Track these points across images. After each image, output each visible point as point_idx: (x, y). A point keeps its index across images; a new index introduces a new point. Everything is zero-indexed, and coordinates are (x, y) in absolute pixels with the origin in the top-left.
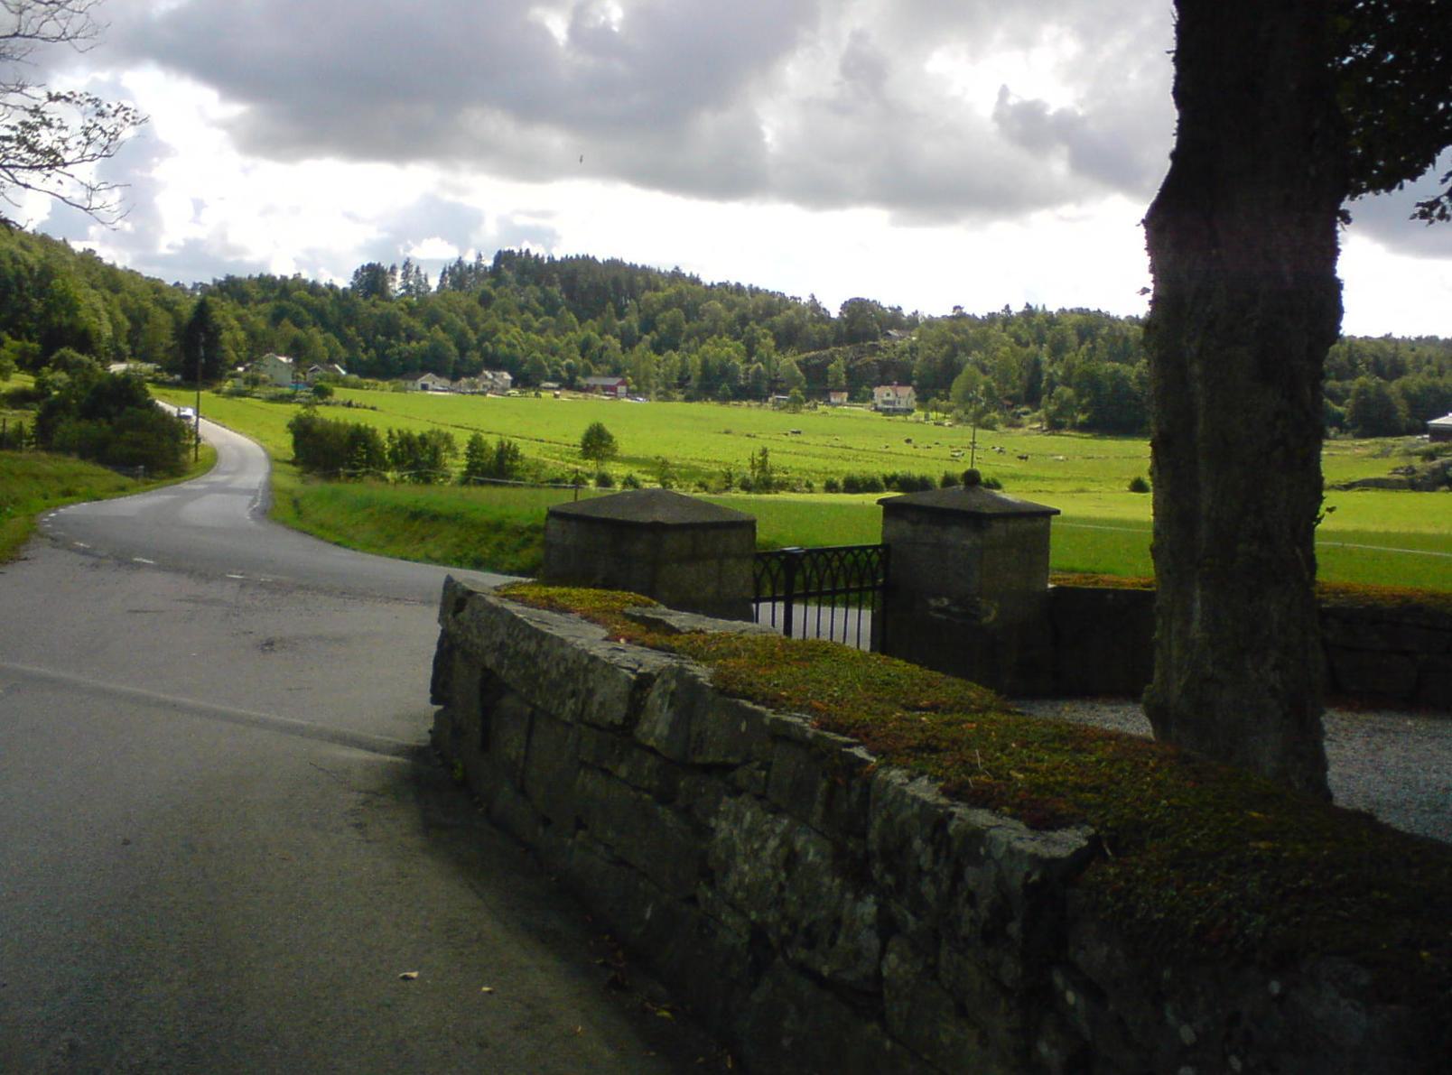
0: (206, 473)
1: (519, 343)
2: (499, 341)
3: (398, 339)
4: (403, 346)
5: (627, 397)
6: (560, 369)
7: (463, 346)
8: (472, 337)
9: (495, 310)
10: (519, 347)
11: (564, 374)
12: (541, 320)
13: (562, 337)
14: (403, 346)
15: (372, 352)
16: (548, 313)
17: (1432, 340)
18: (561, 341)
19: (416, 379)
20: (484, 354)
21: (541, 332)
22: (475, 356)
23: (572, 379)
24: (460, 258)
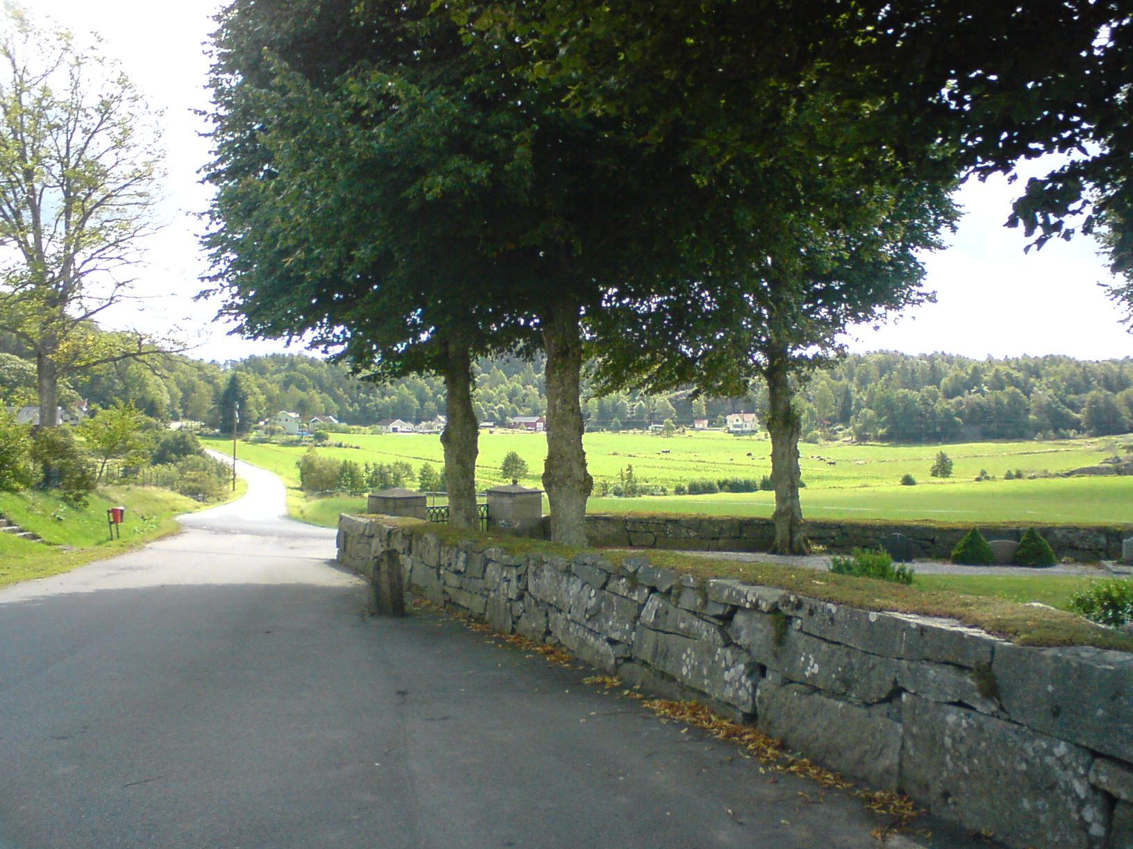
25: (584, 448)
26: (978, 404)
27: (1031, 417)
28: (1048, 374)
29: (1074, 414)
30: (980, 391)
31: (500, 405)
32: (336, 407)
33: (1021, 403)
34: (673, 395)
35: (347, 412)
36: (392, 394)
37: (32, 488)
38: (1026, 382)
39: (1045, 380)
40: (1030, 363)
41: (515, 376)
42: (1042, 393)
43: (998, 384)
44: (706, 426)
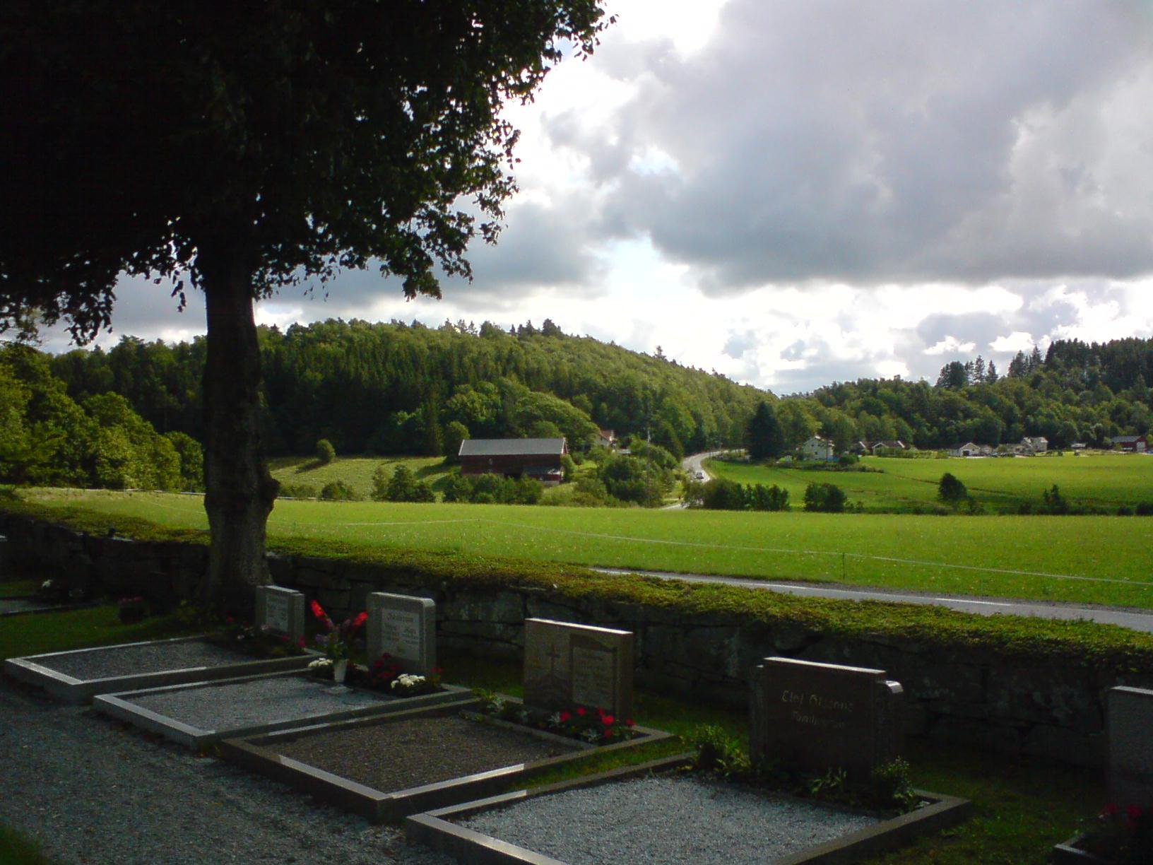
0: (145, 522)
1: (1057, 415)
2: (1041, 413)
3: (957, 418)
4: (961, 423)
5: (1146, 451)
6: (1088, 432)
7: (1009, 419)
8: (1018, 412)
9: (1040, 390)
10: (1056, 417)
11: (1093, 436)
12: (1081, 394)
13: (1096, 406)
14: (961, 423)
15: (935, 429)
16: (1087, 388)
17: (1137, 343)
18: (1095, 410)
19: (958, 448)
20: (1027, 423)
21: (1078, 404)
22: (1019, 427)
23: (1101, 438)
24: (1036, 349)
31: (1098, 424)
32: (911, 431)
35: (925, 436)
36: (976, 417)
41: (1123, 391)
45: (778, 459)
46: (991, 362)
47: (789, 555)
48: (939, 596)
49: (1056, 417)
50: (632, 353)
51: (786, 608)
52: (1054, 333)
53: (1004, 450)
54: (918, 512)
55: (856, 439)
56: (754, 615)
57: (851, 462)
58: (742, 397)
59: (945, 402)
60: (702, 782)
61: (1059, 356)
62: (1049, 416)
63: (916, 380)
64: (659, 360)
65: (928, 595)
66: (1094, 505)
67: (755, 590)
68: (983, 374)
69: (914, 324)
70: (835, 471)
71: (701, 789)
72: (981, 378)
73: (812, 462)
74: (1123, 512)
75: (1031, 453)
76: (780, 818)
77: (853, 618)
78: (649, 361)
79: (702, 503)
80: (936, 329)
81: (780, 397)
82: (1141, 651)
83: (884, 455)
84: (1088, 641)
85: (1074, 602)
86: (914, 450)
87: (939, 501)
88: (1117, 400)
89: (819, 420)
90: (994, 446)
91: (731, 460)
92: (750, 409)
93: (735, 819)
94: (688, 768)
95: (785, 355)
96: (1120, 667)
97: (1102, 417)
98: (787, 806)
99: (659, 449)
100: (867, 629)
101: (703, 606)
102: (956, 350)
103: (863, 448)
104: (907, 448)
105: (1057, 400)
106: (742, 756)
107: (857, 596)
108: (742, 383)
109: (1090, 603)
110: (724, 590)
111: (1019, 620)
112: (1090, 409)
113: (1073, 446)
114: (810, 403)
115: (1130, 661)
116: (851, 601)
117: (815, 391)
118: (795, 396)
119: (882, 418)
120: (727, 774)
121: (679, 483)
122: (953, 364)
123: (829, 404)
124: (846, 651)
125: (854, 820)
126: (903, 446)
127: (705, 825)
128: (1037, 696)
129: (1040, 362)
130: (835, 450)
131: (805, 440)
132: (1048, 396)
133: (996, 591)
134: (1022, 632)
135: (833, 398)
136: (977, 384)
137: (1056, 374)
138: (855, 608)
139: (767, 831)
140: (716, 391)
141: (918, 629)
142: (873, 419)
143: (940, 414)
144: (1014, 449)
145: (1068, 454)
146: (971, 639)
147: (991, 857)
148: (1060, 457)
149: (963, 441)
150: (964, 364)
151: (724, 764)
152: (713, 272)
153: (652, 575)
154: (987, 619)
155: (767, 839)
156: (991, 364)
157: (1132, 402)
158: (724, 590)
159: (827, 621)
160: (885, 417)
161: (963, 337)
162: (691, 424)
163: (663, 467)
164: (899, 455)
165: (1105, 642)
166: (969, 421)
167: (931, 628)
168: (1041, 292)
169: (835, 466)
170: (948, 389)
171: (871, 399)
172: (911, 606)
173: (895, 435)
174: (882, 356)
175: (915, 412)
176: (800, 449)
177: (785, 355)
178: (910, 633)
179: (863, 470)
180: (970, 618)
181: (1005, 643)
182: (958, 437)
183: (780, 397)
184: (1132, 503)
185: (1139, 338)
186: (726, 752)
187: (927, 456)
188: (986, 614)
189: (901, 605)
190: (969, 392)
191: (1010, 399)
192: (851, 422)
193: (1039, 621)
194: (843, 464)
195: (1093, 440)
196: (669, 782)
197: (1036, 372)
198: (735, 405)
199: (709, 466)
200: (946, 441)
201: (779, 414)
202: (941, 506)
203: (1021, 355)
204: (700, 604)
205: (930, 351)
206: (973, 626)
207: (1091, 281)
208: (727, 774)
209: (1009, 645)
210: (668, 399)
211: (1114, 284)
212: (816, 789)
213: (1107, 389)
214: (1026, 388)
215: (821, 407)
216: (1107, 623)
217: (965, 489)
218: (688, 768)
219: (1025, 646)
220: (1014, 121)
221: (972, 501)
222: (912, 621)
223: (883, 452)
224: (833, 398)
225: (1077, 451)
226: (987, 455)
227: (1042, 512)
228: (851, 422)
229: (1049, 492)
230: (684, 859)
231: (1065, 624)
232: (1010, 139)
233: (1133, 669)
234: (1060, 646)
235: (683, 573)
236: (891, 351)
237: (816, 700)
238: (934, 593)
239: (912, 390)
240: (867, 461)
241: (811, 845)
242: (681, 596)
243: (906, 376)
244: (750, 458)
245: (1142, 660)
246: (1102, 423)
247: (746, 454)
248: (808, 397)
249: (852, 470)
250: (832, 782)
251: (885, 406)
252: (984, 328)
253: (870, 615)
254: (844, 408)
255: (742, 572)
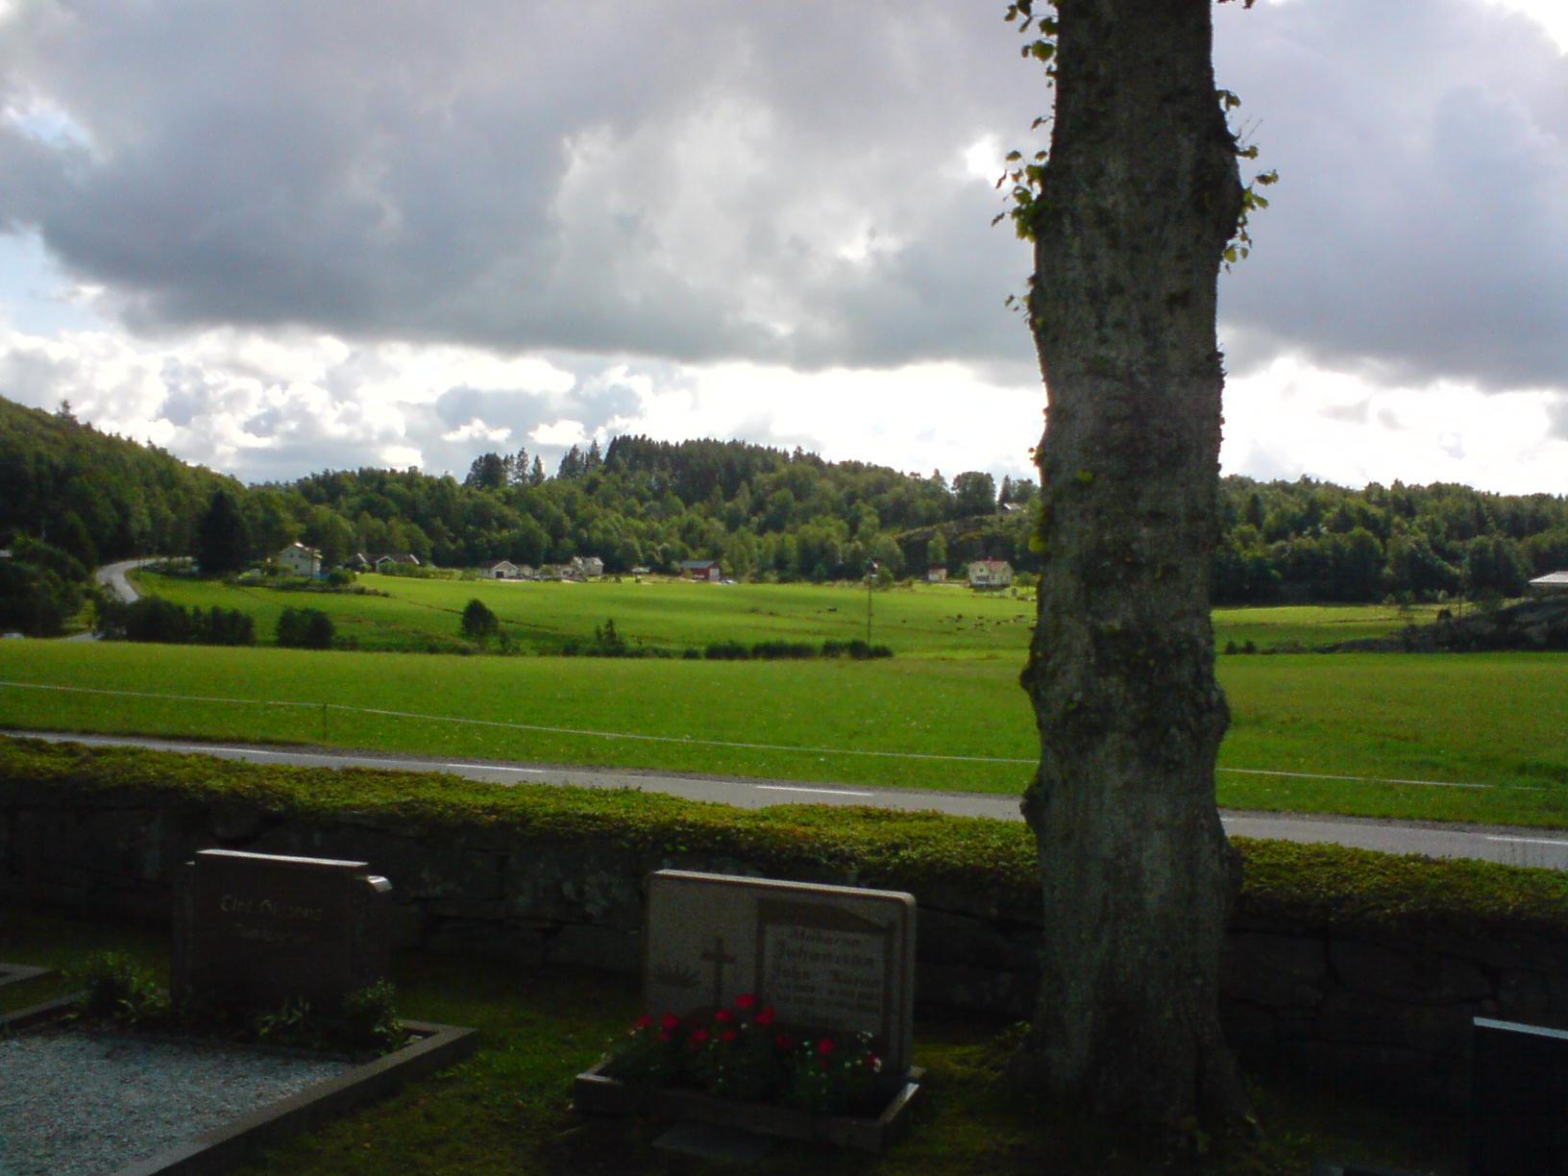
2: (596, 527)
4: (495, 535)
5: (720, 580)
7: (557, 532)
8: (567, 522)
10: (615, 533)
11: (658, 559)
12: (647, 505)
15: (461, 542)
18: (663, 526)
19: (490, 566)
20: (579, 540)
21: (642, 517)
23: (667, 563)
25: (1023, 255)
26: (1308, 551)
27: (1387, 570)
28: (1425, 512)
29: (1452, 569)
30: (1316, 534)
32: (428, 543)
33: (1372, 550)
34: (903, 535)
37: (877, 586)
38: (1388, 521)
39: (1418, 520)
40: (1400, 496)
42: (1411, 538)
43: (1344, 523)
44: (944, 577)
45: (240, 573)
46: (537, 457)
47: (248, 706)
48: (452, 761)
49: (615, 533)
50: (20, 408)
51: (234, 780)
52: (610, 425)
53: (548, 572)
54: (433, 650)
55: (352, 549)
56: (185, 790)
57: (345, 581)
58: (192, 483)
59: (476, 506)
60: (95, 1036)
61: (623, 455)
62: (606, 531)
63: (438, 474)
64: (65, 423)
65: (436, 761)
66: (657, 645)
67: (190, 755)
68: (526, 472)
69: (432, 399)
70: (322, 592)
71: (91, 1047)
72: (523, 477)
73: (290, 579)
74: (690, 655)
75: (581, 576)
76: (211, 1076)
77: (329, 792)
78: (49, 421)
79: (125, 632)
80: (461, 407)
81: (247, 486)
82: (692, 825)
83: (391, 573)
84: (632, 814)
85: (625, 767)
86: (432, 568)
87: (462, 636)
88: (692, 515)
89: (301, 521)
90: (535, 566)
91: (170, 573)
92: (202, 499)
93: (141, 1084)
94: (72, 1016)
95: (251, 427)
96: (668, 847)
97: (670, 535)
98: (224, 1057)
99: (58, 552)
100: (347, 807)
101: (109, 779)
102: (485, 438)
103: (362, 562)
104: (422, 565)
105: (618, 512)
106: (159, 991)
107: (336, 762)
108: (192, 464)
109: (641, 768)
110: (143, 755)
111: (548, 791)
112: (657, 525)
113: (634, 570)
114: (291, 496)
115: (680, 839)
116: (328, 770)
117: (299, 481)
118: (268, 486)
119: (390, 522)
120: (133, 1020)
121: (89, 604)
122: (487, 456)
123: (317, 500)
124: (318, 838)
125: (319, 1068)
126: (417, 562)
127: (92, 1098)
128: (568, 888)
129: (598, 461)
130: (324, 563)
131: (281, 548)
132: (606, 505)
133: (528, 754)
134: (551, 807)
135: (322, 491)
136: (517, 484)
137: (617, 478)
138: (332, 779)
139: (190, 1096)
140: (152, 471)
141: (416, 805)
142: (377, 523)
143: (468, 522)
144: (562, 573)
145: (627, 580)
146: (486, 817)
147: (498, 1100)
148: (618, 585)
149: (497, 558)
150: (503, 458)
151: (130, 1005)
152: (144, 299)
153: (30, 736)
154: (508, 790)
155: (189, 1107)
156: (537, 460)
157: (706, 518)
158: (143, 755)
159: (291, 797)
160: (392, 521)
161: (494, 422)
162: (111, 516)
163: (64, 578)
164: (411, 574)
165: (651, 816)
166: (505, 533)
167: (434, 803)
168: (598, 371)
169: (321, 586)
170: (479, 489)
171: (376, 497)
172: (409, 774)
173: (407, 547)
174: (388, 438)
175: (435, 516)
176: (273, 561)
177: (251, 427)
178: (405, 810)
179: (361, 592)
180: (486, 789)
181: (529, 821)
182: (490, 552)
183: (247, 486)
184: (701, 644)
185: (718, 440)
186: (134, 988)
187: (448, 577)
188: (510, 783)
189: (396, 774)
190: (508, 495)
191: (558, 507)
192: (347, 525)
193: (573, 790)
194: (334, 583)
195: (658, 564)
196: (37, 1042)
197: (593, 473)
198: (180, 493)
199: (137, 579)
200: (473, 557)
201: (244, 509)
202: (465, 643)
203: (575, 450)
204: (104, 777)
205: (451, 437)
206: (488, 800)
207: (653, 363)
208: (133, 1020)
209: (535, 823)
210: (76, 480)
211: (688, 371)
212: (265, 1030)
213: (678, 500)
214: (580, 494)
215: (305, 503)
216: (658, 791)
217: (497, 621)
218: (72, 1016)
219: (556, 824)
220: (567, 142)
221: (504, 638)
222: (408, 794)
223: (390, 568)
224: (322, 491)
225: (639, 577)
226: (526, 577)
227: (593, 653)
228: (347, 525)
229: (603, 628)
230: (50, 1155)
231: (606, 794)
232: (560, 165)
233: (683, 848)
234: (598, 822)
235: (85, 733)
236: (401, 432)
237: (269, 905)
238: (446, 758)
239: (432, 488)
240: (365, 580)
241: (254, 1109)
242: (76, 765)
243: (423, 467)
244: (200, 570)
245: (693, 836)
246: (670, 543)
247: (194, 564)
248: (288, 488)
249: (347, 592)
250: (290, 1017)
251: (393, 506)
252: (522, 411)
253: (352, 788)
254: (338, 508)
255: (177, 731)
